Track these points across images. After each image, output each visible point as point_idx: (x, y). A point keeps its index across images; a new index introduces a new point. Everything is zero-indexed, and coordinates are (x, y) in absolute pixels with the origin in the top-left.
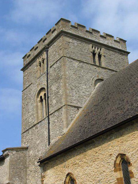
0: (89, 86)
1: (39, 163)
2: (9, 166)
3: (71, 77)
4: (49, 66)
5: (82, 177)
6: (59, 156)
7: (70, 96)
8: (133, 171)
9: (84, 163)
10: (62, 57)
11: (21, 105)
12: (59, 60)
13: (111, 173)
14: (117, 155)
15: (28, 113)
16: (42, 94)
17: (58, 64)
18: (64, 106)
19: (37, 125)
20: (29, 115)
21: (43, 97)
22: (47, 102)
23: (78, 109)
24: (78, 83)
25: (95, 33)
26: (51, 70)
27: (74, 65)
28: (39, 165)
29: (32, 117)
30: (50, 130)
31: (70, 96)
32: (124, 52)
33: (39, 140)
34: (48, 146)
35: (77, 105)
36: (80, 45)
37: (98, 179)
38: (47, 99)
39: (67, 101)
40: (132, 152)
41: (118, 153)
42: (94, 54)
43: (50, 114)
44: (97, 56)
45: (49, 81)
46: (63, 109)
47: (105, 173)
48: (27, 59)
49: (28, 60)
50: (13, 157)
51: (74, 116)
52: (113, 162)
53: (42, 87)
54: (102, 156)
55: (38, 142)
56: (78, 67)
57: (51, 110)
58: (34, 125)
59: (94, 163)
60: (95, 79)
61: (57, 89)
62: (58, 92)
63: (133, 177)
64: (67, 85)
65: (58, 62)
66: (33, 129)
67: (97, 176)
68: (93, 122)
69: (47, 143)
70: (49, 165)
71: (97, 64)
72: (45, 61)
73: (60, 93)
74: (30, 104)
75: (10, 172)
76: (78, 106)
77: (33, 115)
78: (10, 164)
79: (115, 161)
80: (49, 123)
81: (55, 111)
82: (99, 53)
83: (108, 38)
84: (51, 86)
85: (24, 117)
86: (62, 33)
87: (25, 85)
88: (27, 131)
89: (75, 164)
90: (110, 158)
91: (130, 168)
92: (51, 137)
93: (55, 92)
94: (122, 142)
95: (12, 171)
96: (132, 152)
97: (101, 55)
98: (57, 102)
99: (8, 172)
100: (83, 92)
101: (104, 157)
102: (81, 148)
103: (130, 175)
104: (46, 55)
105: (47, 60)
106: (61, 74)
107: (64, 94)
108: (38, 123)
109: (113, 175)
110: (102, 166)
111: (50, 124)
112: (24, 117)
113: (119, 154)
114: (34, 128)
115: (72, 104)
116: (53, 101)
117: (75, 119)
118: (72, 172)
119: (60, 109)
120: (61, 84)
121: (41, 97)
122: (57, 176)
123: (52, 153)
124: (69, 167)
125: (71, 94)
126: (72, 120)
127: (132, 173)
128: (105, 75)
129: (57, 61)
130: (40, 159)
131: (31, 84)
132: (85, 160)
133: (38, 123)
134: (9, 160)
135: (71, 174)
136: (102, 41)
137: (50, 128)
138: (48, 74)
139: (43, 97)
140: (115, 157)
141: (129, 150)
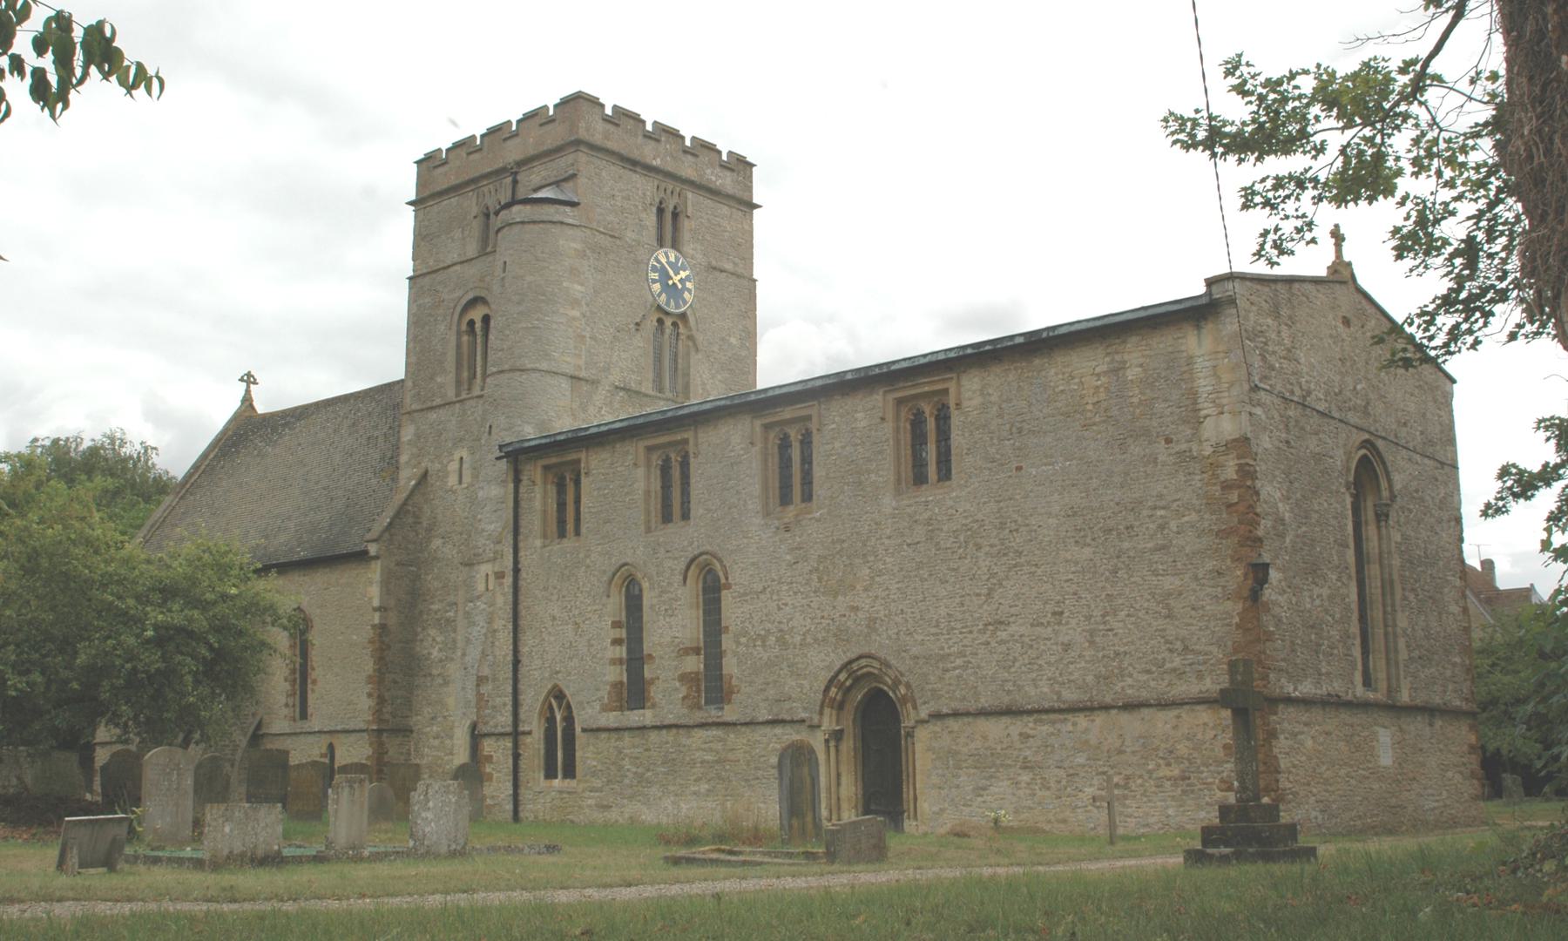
21: (478, 325)
42: (660, 211)
82: (675, 208)
136: (687, 169)
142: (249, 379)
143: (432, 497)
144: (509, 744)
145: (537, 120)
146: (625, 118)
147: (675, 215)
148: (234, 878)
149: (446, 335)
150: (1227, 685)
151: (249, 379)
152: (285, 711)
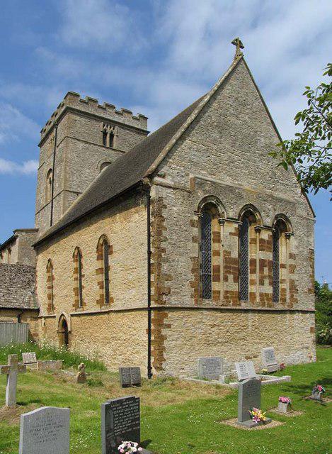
35: (76, 191)
42: (105, 134)
44: (108, 135)
71: (108, 145)
117: (73, 205)
147: (112, 136)
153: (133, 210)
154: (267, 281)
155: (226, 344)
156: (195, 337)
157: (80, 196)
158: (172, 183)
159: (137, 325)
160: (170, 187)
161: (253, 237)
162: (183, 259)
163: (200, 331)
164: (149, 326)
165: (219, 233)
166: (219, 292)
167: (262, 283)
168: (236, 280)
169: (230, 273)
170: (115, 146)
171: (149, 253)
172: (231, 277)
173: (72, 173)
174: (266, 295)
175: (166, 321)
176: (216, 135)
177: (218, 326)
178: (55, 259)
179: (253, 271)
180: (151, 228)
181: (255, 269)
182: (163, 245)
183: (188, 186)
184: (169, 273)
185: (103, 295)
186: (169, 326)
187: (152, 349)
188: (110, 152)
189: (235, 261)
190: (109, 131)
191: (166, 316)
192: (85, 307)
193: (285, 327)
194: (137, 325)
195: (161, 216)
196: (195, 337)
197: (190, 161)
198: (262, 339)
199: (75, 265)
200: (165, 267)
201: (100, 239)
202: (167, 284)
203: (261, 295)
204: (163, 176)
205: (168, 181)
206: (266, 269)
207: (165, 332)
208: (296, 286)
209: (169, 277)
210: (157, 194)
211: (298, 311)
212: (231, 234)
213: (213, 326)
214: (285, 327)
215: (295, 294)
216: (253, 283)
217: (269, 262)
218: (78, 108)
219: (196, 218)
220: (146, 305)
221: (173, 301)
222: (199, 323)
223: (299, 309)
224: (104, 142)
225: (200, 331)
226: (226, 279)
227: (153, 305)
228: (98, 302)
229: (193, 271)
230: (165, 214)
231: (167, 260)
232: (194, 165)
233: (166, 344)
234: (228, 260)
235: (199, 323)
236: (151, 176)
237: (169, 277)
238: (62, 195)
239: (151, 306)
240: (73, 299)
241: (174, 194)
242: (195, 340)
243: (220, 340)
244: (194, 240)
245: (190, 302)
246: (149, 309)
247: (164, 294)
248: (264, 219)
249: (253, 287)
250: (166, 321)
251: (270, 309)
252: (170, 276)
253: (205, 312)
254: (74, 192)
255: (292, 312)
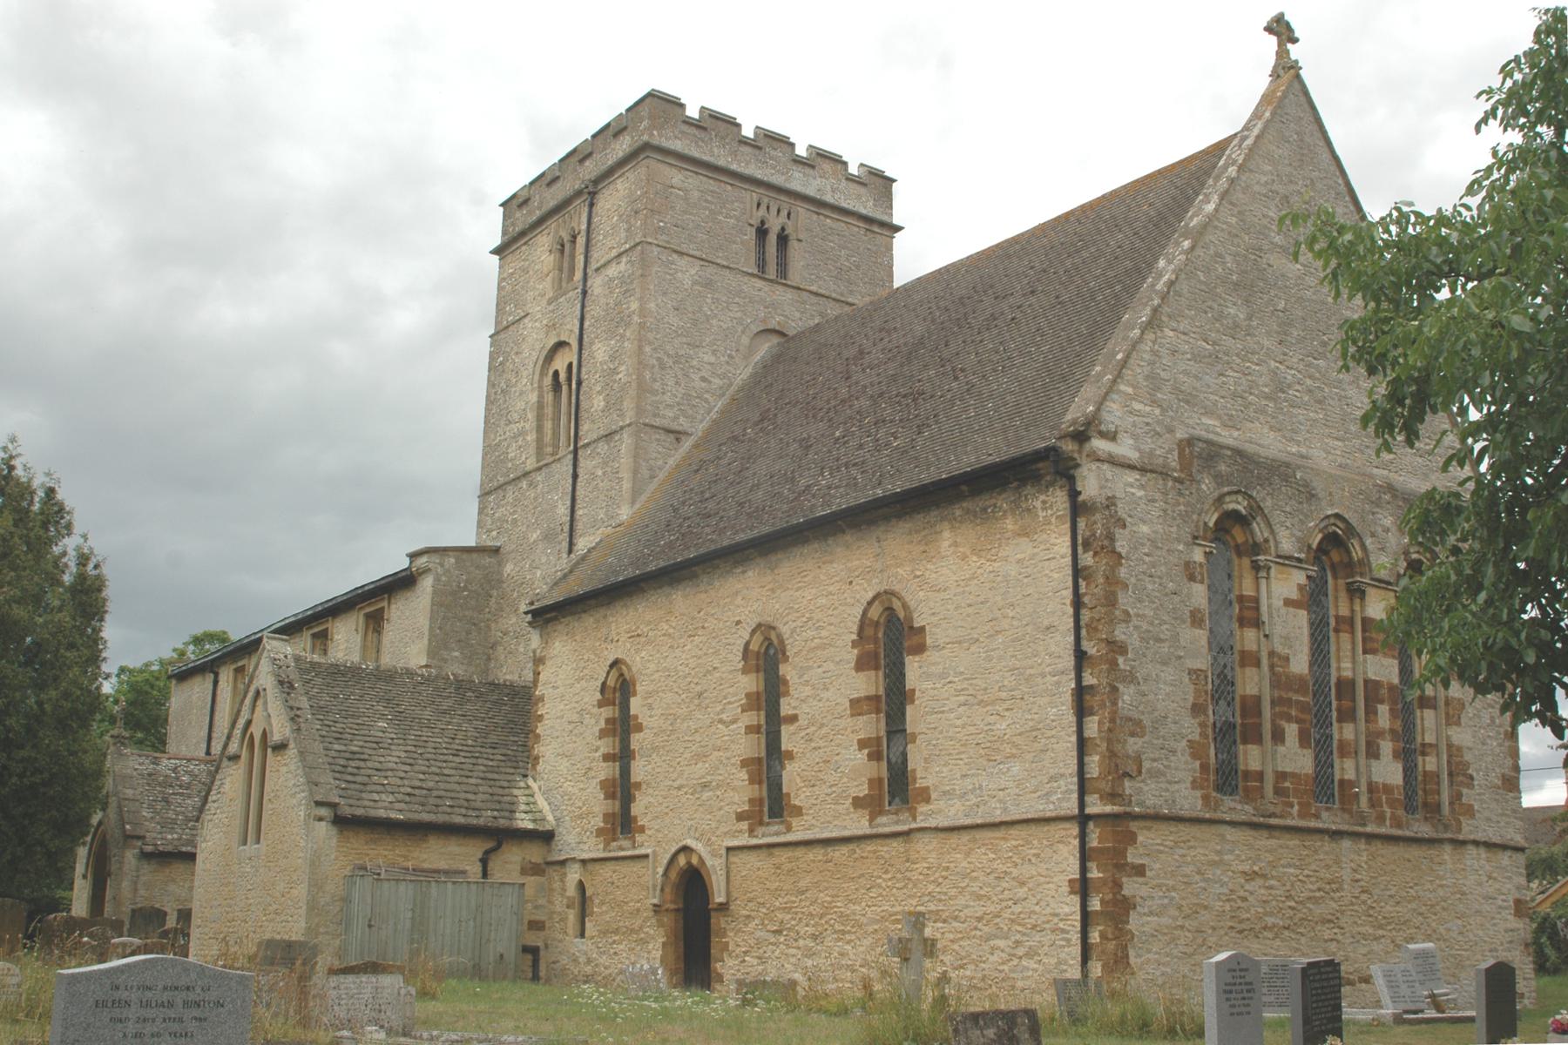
0: (730, 356)
1: (530, 616)
2: (429, 608)
3: (665, 320)
4: (593, 265)
5: (652, 678)
6: (593, 602)
7: (654, 392)
8: (788, 678)
9: (664, 635)
10: (638, 244)
11: (393, 607)
12: (626, 251)
13: (731, 677)
14: (754, 626)
15: (506, 425)
16: (560, 364)
17: (622, 267)
18: (629, 425)
19: (533, 474)
20: (508, 433)
21: (563, 376)
22: (574, 397)
23: (678, 440)
24: (689, 344)
25: (775, 149)
26: (597, 284)
27: (679, 274)
28: (529, 623)
29: (520, 443)
30: (578, 501)
31: (654, 392)
32: (883, 224)
33: (539, 532)
34: (565, 555)
35: (675, 427)
36: (709, 198)
37: (699, 688)
38: (574, 386)
39: (640, 411)
40: (795, 624)
41: (757, 620)
42: (762, 232)
43: (580, 444)
44: (772, 239)
45: (587, 324)
46: (625, 436)
47: (718, 675)
48: (518, 215)
49: (524, 218)
50: (443, 579)
51: (660, 463)
52: (741, 643)
53: (562, 339)
54: (715, 622)
55: (535, 536)
56: (695, 283)
57: (588, 431)
58: (526, 474)
59: (690, 640)
60: (755, 329)
61: (613, 358)
62: (615, 371)
63: (787, 693)
64: (648, 349)
65: (624, 259)
66: (520, 486)
67: (695, 681)
68: (711, 505)
69: (565, 545)
70: (560, 627)
71: (772, 271)
72: (581, 240)
73: (620, 376)
74: (515, 392)
75: (431, 629)
76: (680, 428)
77: (522, 433)
78: (433, 605)
79: (747, 644)
80: (575, 476)
81: (599, 439)
82: (783, 229)
83: (827, 166)
84: (592, 344)
85: (492, 436)
86: (642, 150)
87: (504, 314)
88: (500, 491)
89: (638, 635)
90: (734, 630)
91: (783, 669)
92: (579, 526)
93: (605, 367)
94: (773, 590)
95: (440, 628)
96: (795, 624)
97: (787, 236)
98: (607, 408)
99: (426, 630)
100: (703, 379)
101: (721, 625)
102: (660, 588)
103: (782, 688)
104: (584, 219)
105: (588, 241)
106: (628, 308)
107: (634, 385)
108: (539, 469)
109: (738, 682)
110: (711, 651)
111: (579, 480)
112: (492, 436)
113: (759, 625)
114: (524, 484)
115: (658, 422)
116: (595, 402)
117: (661, 475)
118: (628, 660)
119: (615, 432)
120: (626, 344)
121: (556, 373)
122: (582, 664)
123: (575, 587)
124: (620, 643)
125: (657, 386)
126: (652, 477)
127: (786, 683)
128: (794, 314)
129: (620, 255)
130: (532, 603)
131: (525, 316)
132: (666, 627)
133: (539, 469)
134: (429, 590)
135: (625, 663)
136: (798, 181)
137: (578, 493)
138: (584, 293)
139: (563, 376)
140: (750, 631)
141: (788, 614)
142: (1280, 29)
143: (101, 647)
144: (1075, 830)
145: (515, 202)
146: (718, 124)
147: (783, 239)
148: (1027, 1036)
149: (527, 393)
150: (866, 792)
151: (1280, 29)
152: (1093, 765)
153: (1010, 524)
154: (1386, 747)
155: (1286, 933)
156: (1206, 908)
157: (687, 444)
158: (1133, 456)
159: (1026, 871)
160: (1132, 467)
161: (1344, 611)
162: (1169, 674)
163: (1217, 889)
164: (1084, 869)
165: (1256, 600)
166: (1260, 776)
167: (1373, 753)
168: (1304, 739)
169: (1289, 719)
170: (795, 277)
171: (1080, 656)
172: (1291, 730)
173: (662, 367)
174: (1388, 789)
175: (1133, 857)
176: (1236, 311)
177: (1264, 876)
178: (642, 663)
179: (1347, 715)
180: (1082, 584)
181: (1354, 710)
182: (1120, 633)
183: (1173, 461)
184: (1136, 715)
185: (880, 780)
186: (1140, 871)
187: (1095, 937)
188: (783, 295)
189: (1299, 684)
190: (774, 225)
191: (1131, 838)
192: (795, 822)
193: (1441, 892)
194: (1026, 871)
195: (1114, 551)
196: (1206, 908)
197: (1177, 390)
198: (1381, 927)
199: (867, 684)
200: (1127, 695)
201: (870, 603)
202: (1133, 745)
203: (1372, 788)
204: (1112, 437)
205: (1124, 448)
206: (1383, 710)
207: (1130, 887)
208: (1467, 765)
209: (1137, 728)
210: (1102, 487)
211: (1476, 843)
212: (1288, 602)
213: (1251, 876)
214: (1441, 892)
215: (1465, 791)
216: (1344, 749)
217: (1391, 688)
218: (677, 145)
219: (1198, 556)
220: (1071, 806)
221: (1147, 794)
222: (1213, 864)
223: (1480, 836)
224: (762, 264)
225: (1217, 889)
226: (1278, 736)
227: (1095, 806)
228: (600, 832)
229: (1197, 709)
230: (1122, 546)
231: (1131, 678)
232: (1187, 402)
233: (1134, 922)
234: (1280, 681)
235: (1213, 864)
236: (1081, 437)
237: (1137, 728)
238: (626, 442)
239: (1088, 811)
240: (740, 791)
241: (1142, 487)
242: (1205, 916)
243: (1270, 920)
244: (1196, 619)
245: (1189, 801)
246: (1083, 819)
247: (1127, 775)
248: (1372, 559)
249: (1349, 764)
250: (1133, 857)
251: (1399, 832)
252: (1139, 723)
253: (1231, 834)
254: (669, 431)
255: (1459, 844)
